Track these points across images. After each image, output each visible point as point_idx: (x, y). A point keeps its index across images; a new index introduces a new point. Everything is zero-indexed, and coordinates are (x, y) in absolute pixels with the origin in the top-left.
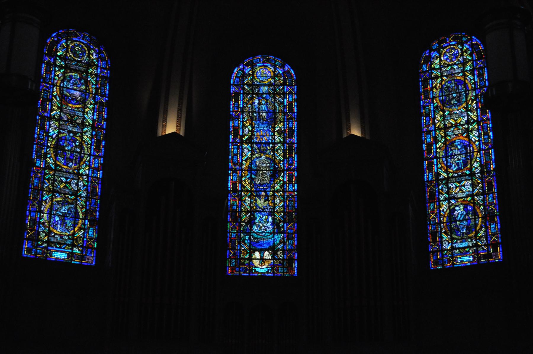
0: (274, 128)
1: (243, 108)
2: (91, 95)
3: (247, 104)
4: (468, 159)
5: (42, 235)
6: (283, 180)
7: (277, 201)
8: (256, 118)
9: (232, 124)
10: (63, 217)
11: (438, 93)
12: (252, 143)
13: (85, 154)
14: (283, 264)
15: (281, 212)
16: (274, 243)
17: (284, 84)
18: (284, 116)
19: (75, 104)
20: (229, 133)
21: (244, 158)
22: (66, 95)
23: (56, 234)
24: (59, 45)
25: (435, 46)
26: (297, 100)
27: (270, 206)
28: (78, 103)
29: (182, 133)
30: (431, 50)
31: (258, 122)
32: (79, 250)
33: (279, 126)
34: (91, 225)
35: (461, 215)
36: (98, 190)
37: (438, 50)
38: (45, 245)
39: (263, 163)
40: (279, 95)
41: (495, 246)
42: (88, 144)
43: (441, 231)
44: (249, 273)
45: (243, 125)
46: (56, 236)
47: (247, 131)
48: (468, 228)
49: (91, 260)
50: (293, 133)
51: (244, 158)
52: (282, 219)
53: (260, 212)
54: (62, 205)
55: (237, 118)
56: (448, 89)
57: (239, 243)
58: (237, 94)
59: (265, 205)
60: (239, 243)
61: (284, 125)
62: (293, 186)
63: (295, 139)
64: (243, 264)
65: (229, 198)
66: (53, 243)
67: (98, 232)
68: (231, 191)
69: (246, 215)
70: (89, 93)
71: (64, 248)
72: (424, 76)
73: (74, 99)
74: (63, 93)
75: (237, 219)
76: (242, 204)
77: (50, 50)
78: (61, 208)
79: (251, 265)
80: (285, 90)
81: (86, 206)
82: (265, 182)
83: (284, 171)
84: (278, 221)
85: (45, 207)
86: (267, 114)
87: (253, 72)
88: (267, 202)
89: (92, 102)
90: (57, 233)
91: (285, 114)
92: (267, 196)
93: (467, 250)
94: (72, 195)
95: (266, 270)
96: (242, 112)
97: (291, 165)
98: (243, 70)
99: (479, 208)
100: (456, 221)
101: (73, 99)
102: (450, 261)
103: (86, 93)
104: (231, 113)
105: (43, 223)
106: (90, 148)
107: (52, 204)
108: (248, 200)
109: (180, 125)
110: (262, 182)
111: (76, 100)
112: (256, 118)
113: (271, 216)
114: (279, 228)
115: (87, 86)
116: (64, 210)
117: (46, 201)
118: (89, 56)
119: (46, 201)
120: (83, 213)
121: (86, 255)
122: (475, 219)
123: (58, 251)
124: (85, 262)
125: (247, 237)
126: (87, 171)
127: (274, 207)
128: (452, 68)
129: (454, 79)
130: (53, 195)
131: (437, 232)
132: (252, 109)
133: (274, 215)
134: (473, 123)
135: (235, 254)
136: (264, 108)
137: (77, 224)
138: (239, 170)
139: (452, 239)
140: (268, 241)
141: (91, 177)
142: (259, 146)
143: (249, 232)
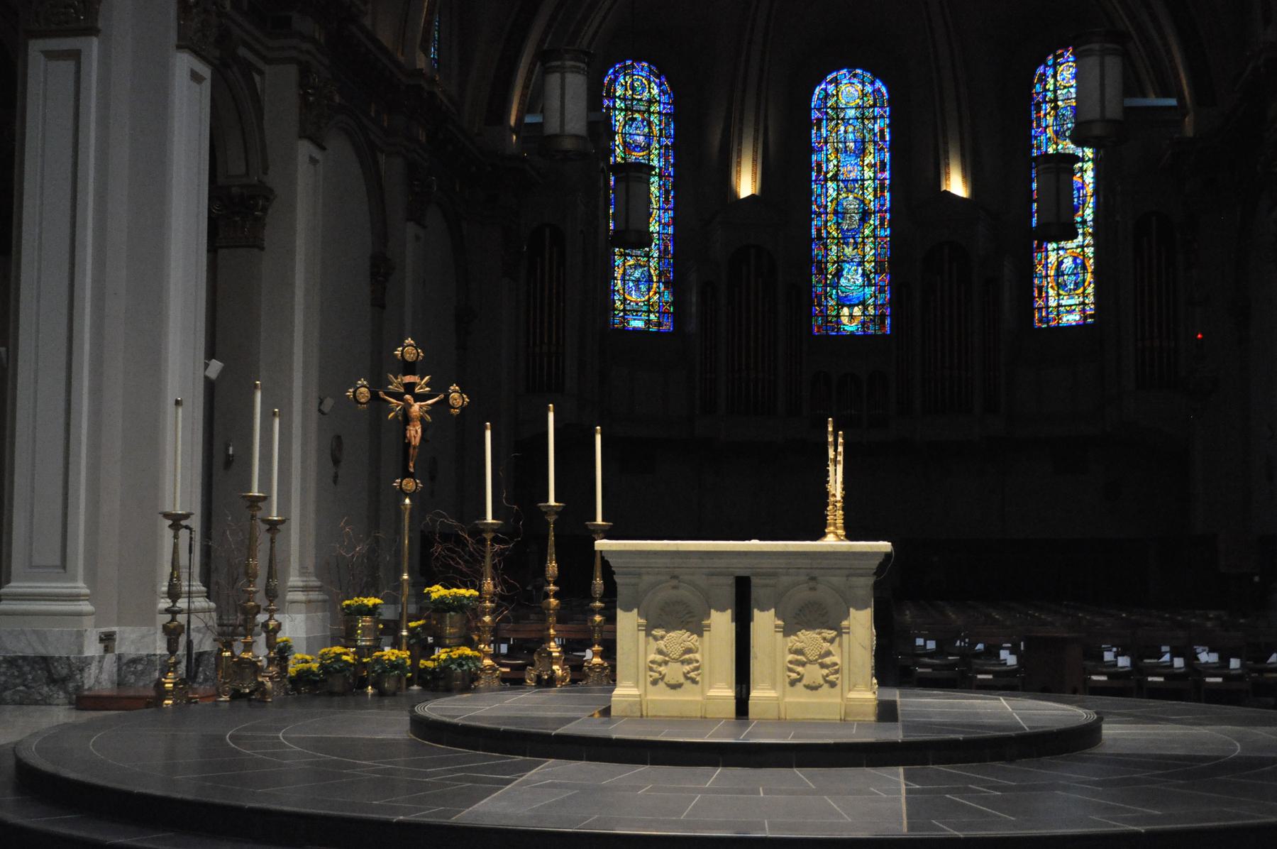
0: (863, 161)
1: (826, 138)
2: (655, 138)
3: (831, 133)
4: (1080, 204)
5: (618, 304)
6: (874, 224)
7: (867, 249)
8: (842, 150)
9: (814, 158)
10: (638, 281)
11: (1052, 120)
12: (838, 181)
13: (653, 208)
15: (871, 261)
16: (864, 298)
17: (874, 106)
18: (875, 145)
19: (639, 152)
20: (811, 169)
21: (829, 199)
22: (629, 143)
23: (631, 301)
24: (617, 84)
25: (1050, 61)
26: (889, 126)
27: (859, 255)
28: (643, 149)
30: (1046, 66)
31: (844, 155)
32: (656, 316)
33: (869, 159)
34: (666, 288)
35: (1070, 269)
36: (670, 248)
37: (1055, 66)
38: (622, 314)
39: (850, 205)
40: (869, 119)
42: (656, 197)
43: (1048, 286)
44: (837, 332)
45: (827, 159)
46: (632, 304)
47: (832, 166)
48: (1076, 284)
49: (668, 326)
50: (885, 167)
51: (829, 199)
52: (873, 270)
53: (848, 262)
54: (635, 268)
55: (821, 150)
56: (1063, 117)
57: (826, 299)
58: (819, 121)
59: (854, 254)
60: (826, 299)
61: (874, 157)
62: (885, 231)
63: (887, 174)
64: (831, 322)
65: (813, 247)
66: (629, 311)
67: (674, 294)
68: (815, 238)
69: (832, 266)
70: (653, 136)
71: (641, 316)
73: (638, 147)
74: (626, 140)
75: (822, 271)
76: (827, 253)
77: (608, 92)
78: (634, 272)
79: (839, 323)
80: (876, 114)
81: (659, 267)
82: (853, 227)
83: (874, 213)
84: (869, 273)
86: (855, 144)
87: (838, 92)
88: (856, 250)
89: (657, 146)
90: (633, 299)
91: (875, 143)
92: (856, 243)
93: (1073, 307)
94: (643, 257)
95: (855, 328)
96: (826, 143)
97: (883, 205)
98: (825, 90)
99: (1088, 262)
100: (1063, 275)
102: (1055, 320)
103: (648, 136)
104: (813, 145)
105: (618, 291)
106: (659, 201)
107: (625, 269)
108: (834, 248)
109: (756, 169)
110: (850, 228)
111: (640, 147)
112: (842, 150)
113: (861, 266)
114: (869, 280)
115: (650, 128)
116: (637, 274)
117: (618, 266)
118: (649, 92)
119: (618, 266)
120: (656, 276)
121: (663, 321)
122: (1084, 273)
123: (635, 319)
125: (834, 291)
126: (657, 228)
127: (864, 256)
128: (1069, 91)
129: (1070, 106)
130: (626, 259)
131: (1043, 286)
132: (837, 138)
133: (864, 266)
134: (1088, 161)
135: (821, 311)
136: (851, 136)
137: (652, 288)
138: (824, 213)
139: (1059, 295)
140: (856, 294)
141: (662, 233)
142: (846, 183)
143: (836, 286)
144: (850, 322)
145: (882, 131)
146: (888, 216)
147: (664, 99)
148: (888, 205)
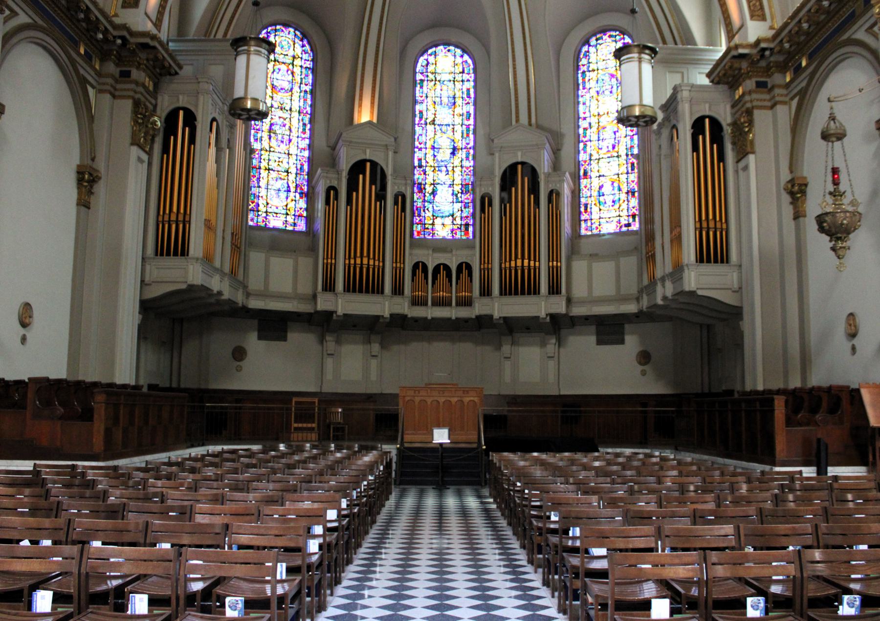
9: (418, 107)
12: (434, 124)
14: (460, 229)
26: (475, 87)
29: (375, 121)
34: (301, 197)
41: (634, 216)
63: (471, 122)
64: (428, 229)
67: (307, 203)
72: (583, 69)
75: (421, 189)
85: (263, 183)
92: (447, 171)
101: (282, 89)
108: (431, 174)
114: (457, 198)
124: (297, 229)
144: (443, 231)
145: (468, 90)
146: (472, 151)
147: (305, 56)
148: (472, 144)
